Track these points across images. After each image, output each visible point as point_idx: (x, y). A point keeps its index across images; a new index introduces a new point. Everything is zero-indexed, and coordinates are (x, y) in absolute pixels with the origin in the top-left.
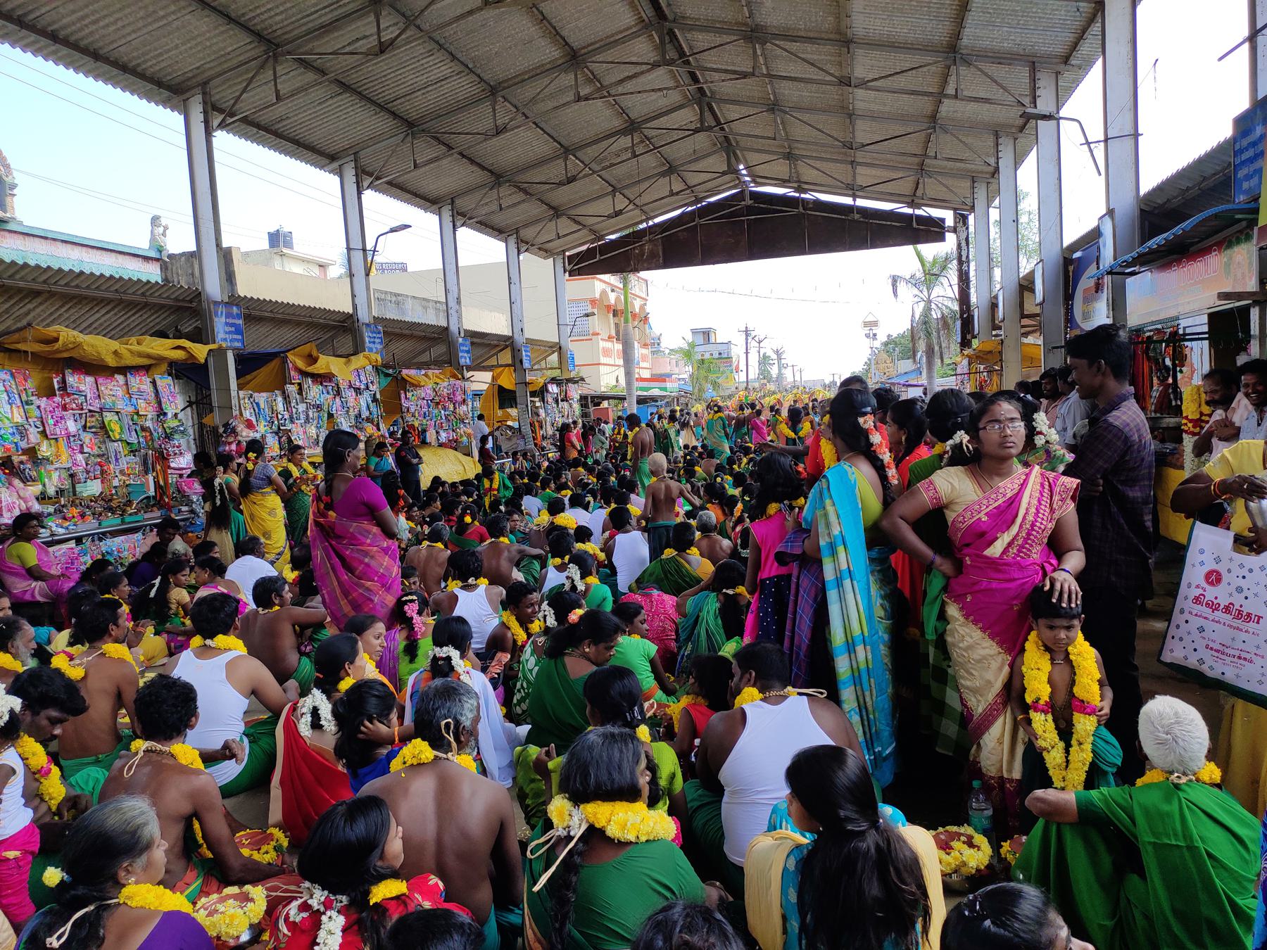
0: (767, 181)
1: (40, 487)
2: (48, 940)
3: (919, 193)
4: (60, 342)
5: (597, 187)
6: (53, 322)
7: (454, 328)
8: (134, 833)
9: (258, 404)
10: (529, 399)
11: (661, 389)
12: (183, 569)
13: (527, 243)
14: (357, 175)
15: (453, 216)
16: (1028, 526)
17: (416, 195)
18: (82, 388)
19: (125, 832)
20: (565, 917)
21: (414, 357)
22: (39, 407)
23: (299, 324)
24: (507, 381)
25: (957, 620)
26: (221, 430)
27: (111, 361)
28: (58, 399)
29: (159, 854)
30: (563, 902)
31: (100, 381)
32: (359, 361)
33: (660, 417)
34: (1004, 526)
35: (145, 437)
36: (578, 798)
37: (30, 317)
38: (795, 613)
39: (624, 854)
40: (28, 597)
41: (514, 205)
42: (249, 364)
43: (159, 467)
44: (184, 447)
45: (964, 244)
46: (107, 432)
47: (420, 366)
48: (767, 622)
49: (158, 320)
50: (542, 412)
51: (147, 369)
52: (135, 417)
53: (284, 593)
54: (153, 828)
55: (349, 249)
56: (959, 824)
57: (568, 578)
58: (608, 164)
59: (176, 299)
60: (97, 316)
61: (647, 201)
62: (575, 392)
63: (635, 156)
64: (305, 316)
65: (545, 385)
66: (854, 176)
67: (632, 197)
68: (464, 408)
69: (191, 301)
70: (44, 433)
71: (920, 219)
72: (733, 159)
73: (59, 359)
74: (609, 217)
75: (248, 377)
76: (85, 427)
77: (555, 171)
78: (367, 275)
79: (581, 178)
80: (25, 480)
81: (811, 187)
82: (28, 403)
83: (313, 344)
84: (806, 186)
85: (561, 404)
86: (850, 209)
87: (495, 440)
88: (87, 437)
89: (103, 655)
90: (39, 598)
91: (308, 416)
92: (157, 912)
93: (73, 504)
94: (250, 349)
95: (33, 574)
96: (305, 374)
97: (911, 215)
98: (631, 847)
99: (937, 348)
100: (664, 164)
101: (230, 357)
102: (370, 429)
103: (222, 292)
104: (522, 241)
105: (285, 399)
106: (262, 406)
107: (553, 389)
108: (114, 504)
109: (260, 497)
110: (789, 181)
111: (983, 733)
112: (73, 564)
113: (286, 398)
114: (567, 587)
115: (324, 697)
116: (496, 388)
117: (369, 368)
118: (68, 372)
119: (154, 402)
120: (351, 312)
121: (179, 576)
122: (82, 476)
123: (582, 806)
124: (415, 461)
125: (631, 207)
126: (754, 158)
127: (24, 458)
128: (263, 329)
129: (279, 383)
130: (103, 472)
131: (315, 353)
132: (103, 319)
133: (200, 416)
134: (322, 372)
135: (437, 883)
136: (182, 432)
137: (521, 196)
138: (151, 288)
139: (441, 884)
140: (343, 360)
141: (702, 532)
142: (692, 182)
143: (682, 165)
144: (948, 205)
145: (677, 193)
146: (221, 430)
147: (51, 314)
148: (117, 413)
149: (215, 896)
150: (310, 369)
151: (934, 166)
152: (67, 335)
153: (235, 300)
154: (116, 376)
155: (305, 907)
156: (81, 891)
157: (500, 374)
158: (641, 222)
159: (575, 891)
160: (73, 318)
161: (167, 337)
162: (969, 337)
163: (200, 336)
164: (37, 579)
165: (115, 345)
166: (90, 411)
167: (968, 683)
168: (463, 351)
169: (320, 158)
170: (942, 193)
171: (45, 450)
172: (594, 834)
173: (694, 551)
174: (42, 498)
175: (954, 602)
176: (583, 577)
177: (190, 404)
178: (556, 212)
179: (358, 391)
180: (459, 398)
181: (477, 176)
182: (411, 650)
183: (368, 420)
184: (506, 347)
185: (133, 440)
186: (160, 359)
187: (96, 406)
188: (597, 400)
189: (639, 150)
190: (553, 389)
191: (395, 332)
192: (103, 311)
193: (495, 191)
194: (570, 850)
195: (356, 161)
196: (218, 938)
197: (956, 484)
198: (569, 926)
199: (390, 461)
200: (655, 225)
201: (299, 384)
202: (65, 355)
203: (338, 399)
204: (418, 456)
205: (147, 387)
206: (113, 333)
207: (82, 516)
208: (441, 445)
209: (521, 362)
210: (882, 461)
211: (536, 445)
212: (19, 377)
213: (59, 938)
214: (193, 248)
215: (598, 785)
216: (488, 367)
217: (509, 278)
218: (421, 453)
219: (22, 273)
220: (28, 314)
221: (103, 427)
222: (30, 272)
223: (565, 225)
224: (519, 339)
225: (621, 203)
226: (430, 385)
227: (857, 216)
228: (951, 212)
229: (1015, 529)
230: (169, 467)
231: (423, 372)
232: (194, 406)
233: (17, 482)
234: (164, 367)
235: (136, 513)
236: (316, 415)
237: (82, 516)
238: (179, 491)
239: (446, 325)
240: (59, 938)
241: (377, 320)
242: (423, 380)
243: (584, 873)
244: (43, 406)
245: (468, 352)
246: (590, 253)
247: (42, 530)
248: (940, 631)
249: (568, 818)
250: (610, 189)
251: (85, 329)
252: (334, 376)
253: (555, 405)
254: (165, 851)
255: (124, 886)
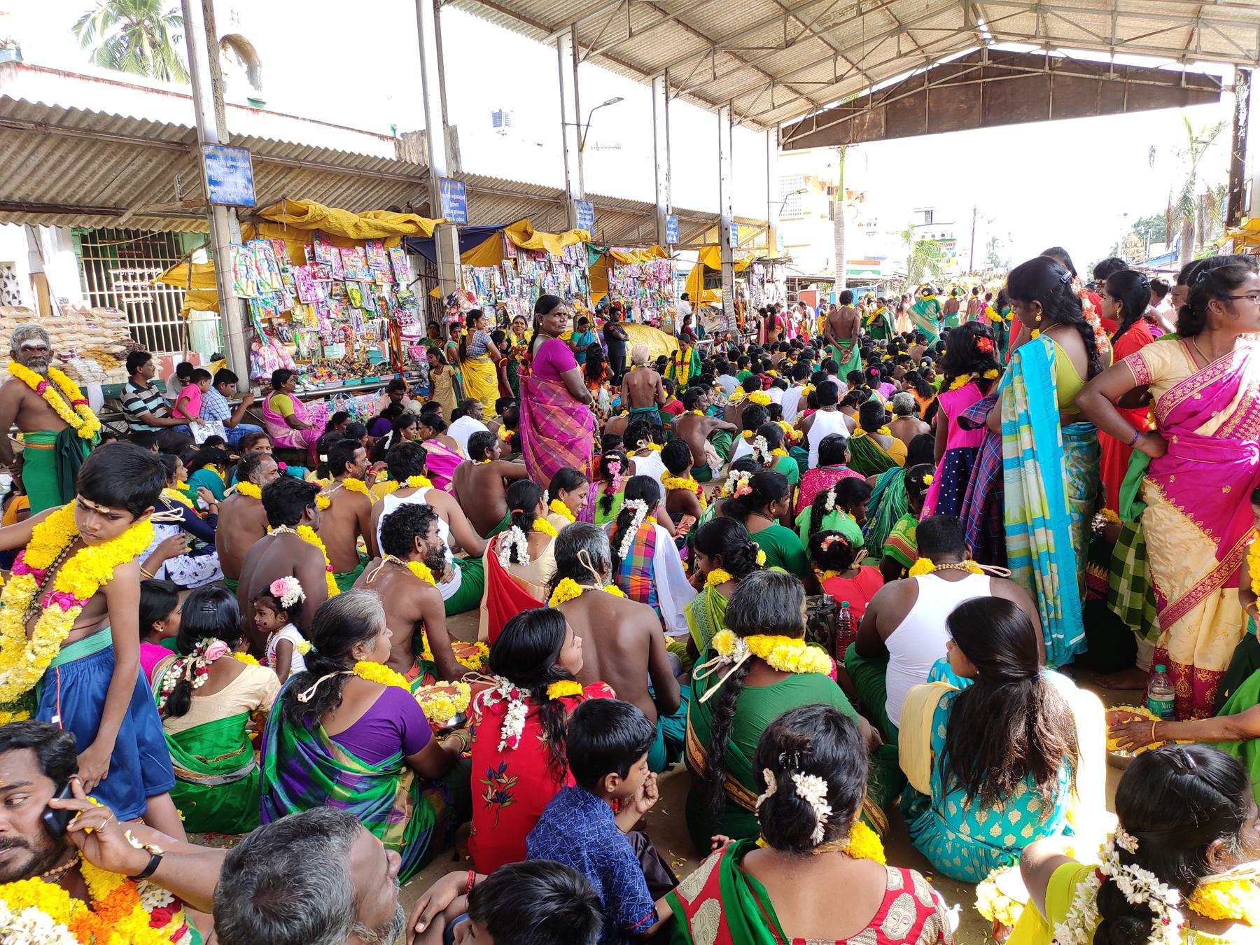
0: (1010, 38)
1: (295, 347)
2: (300, 696)
3: (1192, 46)
4: (309, 215)
5: (818, 50)
6: (303, 197)
7: (662, 204)
8: (365, 620)
9: (477, 278)
10: (734, 280)
11: (873, 272)
12: (411, 423)
13: (740, 115)
14: (574, 47)
15: (666, 87)
16: (1248, 404)
17: (630, 66)
18: (328, 258)
19: (356, 618)
20: (724, 730)
21: (623, 235)
22: (293, 275)
23: (516, 200)
24: (713, 263)
25: (1156, 502)
26: (445, 302)
27: (352, 234)
28: (308, 268)
29: (385, 639)
30: (723, 716)
31: (343, 252)
32: (570, 238)
33: (869, 302)
34: (1221, 405)
35: (382, 306)
36: (743, 631)
37: (284, 192)
38: (975, 482)
39: (782, 681)
40: (286, 443)
41: (729, 73)
42: (471, 238)
43: (393, 334)
44: (414, 316)
45: (1243, 105)
46: (349, 301)
47: (628, 245)
48: (948, 493)
49: (392, 196)
50: (747, 294)
51: (382, 242)
52: (373, 287)
53: (494, 448)
54: (379, 618)
55: (564, 124)
56: (1136, 705)
57: (755, 449)
58: (831, 24)
59: (408, 176)
60: (341, 191)
61: (872, 64)
62: (781, 274)
63: (861, 14)
64: (521, 193)
65: (751, 266)
66: (1114, 29)
67: (856, 61)
68: (669, 286)
69: (421, 178)
70: (297, 299)
71: (1191, 77)
72: (971, 14)
73: (309, 231)
74: (830, 83)
75: (470, 252)
76: (331, 295)
77: (774, 34)
78: (581, 150)
79: (799, 41)
80: (282, 340)
81: (1061, 43)
82: (284, 271)
83: (528, 221)
84: (1055, 43)
85: (767, 285)
86: (1106, 67)
87: (698, 318)
88: (333, 304)
89: (344, 487)
90: (295, 445)
91: (522, 290)
92: (382, 685)
93: (322, 364)
94: (472, 225)
95: (291, 423)
96: (520, 249)
97: (1181, 73)
98: (789, 676)
99: (1196, 231)
100: (892, 22)
101: (455, 232)
102: (578, 304)
103: (448, 169)
104: (735, 113)
105: (502, 273)
106: (481, 280)
107: (759, 269)
108: (355, 366)
109: (478, 364)
110: (1035, 37)
111: (1175, 621)
112: (322, 417)
113: (503, 273)
114: (755, 457)
115: (523, 535)
116: (702, 267)
117: (580, 244)
118: (316, 243)
119: (389, 273)
120: (564, 189)
121: (408, 429)
122: (329, 339)
123: (745, 638)
124: (622, 336)
125: (854, 71)
126: (996, 11)
127: (282, 321)
128: (484, 205)
129: (497, 258)
130: (346, 336)
131: (529, 229)
132: (345, 194)
133: (428, 289)
134: (535, 247)
135: (609, 692)
136: (413, 302)
137: (737, 63)
138: (385, 165)
139: (613, 692)
140: (555, 236)
141: (899, 414)
142: (922, 42)
143: (914, 22)
144: (1227, 59)
145: (906, 55)
146: (445, 302)
147: (301, 189)
148: (358, 282)
149: (429, 687)
150: (525, 245)
151: (1213, 14)
152: (315, 207)
153: (458, 177)
154: (357, 248)
155: (496, 695)
156: (324, 661)
157: (708, 252)
158: (863, 88)
159: (734, 709)
160: (320, 193)
161: (399, 211)
162: (1237, 215)
163: (425, 212)
164: (293, 427)
165: (355, 218)
166: (335, 280)
167: (1162, 568)
168: (670, 229)
169: (540, 30)
170: (1222, 46)
171: (299, 314)
172: (755, 662)
173: (885, 429)
174: (297, 356)
175: (1156, 483)
176: (770, 449)
177: (420, 277)
178: (773, 79)
179: (568, 267)
180: (664, 277)
181: (693, 43)
182: (607, 503)
183: (577, 295)
184: (714, 225)
185: (371, 307)
186: (394, 233)
187: (340, 277)
188: (804, 283)
189: (865, 8)
190: (759, 269)
191: (604, 208)
192: (345, 187)
193: (710, 59)
194: (734, 673)
195: (573, 31)
196: (431, 720)
197: (1168, 359)
198: (726, 739)
199: (596, 336)
200: (879, 91)
201: (515, 259)
202: (314, 227)
203: (549, 275)
204: (623, 332)
205: (383, 259)
206: (354, 207)
207: (330, 375)
208: (647, 323)
209: (728, 240)
210: (1091, 327)
211: (739, 326)
212: (277, 246)
213: (308, 695)
214: (423, 127)
215: (766, 622)
216: (695, 246)
217: (720, 153)
218: (627, 330)
219: (278, 150)
220: (282, 188)
221: (346, 295)
222: (284, 148)
223: (781, 94)
224: (727, 216)
225: (843, 67)
226: (637, 263)
227: (1113, 76)
228: (1232, 68)
229: (1232, 408)
230: (401, 334)
231: (631, 250)
232: (423, 279)
233: (276, 342)
234: (398, 240)
235: (374, 375)
236: (529, 289)
237: (330, 375)
238: (410, 357)
239: (654, 202)
240: (308, 695)
241: (589, 197)
242: (630, 257)
243: (744, 695)
244: (296, 274)
245: (675, 230)
246: (806, 124)
247: (297, 386)
248: (1136, 515)
249: (732, 646)
250: (832, 52)
251: (330, 204)
252: (546, 251)
253: (760, 287)
254: (390, 639)
255: (357, 661)
